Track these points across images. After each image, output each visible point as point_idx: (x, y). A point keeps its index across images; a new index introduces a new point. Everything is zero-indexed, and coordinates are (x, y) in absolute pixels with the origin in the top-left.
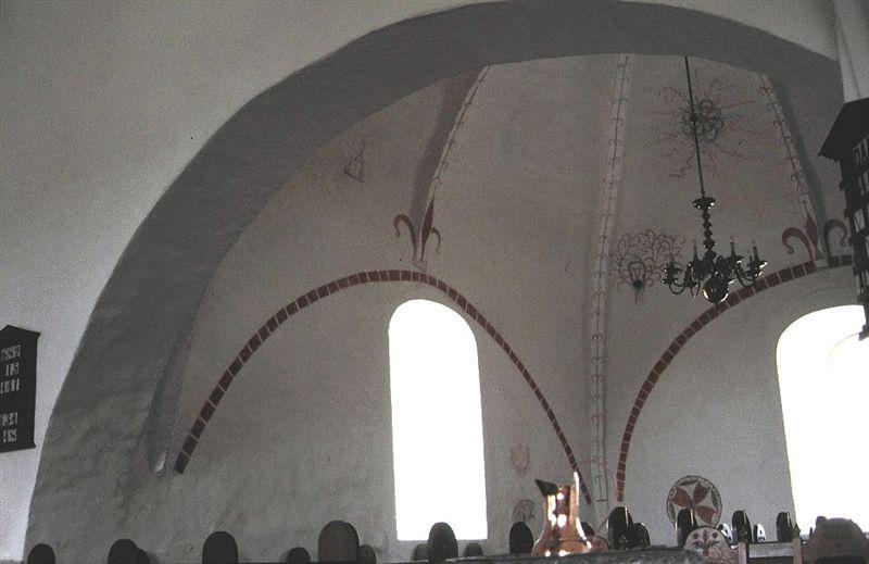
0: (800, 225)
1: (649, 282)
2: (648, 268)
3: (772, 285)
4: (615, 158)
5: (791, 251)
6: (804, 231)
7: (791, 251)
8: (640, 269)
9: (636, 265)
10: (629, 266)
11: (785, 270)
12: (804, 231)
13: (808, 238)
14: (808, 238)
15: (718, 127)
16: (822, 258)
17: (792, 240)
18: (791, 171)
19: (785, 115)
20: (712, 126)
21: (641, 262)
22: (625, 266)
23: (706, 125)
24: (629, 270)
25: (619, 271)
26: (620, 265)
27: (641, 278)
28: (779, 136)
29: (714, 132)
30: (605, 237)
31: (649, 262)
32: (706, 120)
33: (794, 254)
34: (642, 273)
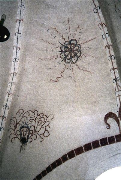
0: (116, 112)
1: (30, 140)
2: (31, 132)
3: (95, 147)
4: (16, 58)
5: (109, 127)
6: (117, 114)
7: (109, 127)
8: (26, 132)
9: (25, 129)
10: (21, 128)
11: (103, 139)
12: (117, 114)
13: (119, 119)
14: (119, 119)
15: (78, 55)
16: (104, 39)
17: (110, 120)
18: (111, 67)
19: (112, 42)
20: (76, 55)
21: (28, 128)
22: (18, 128)
23: (73, 54)
24: (20, 131)
25: (14, 131)
26: (16, 127)
27: (26, 137)
28: (108, 55)
29: (76, 58)
30: (6, 106)
31: (32, 128)
32: (73, 51)
33: (107, 130)
34: (27, 134)
